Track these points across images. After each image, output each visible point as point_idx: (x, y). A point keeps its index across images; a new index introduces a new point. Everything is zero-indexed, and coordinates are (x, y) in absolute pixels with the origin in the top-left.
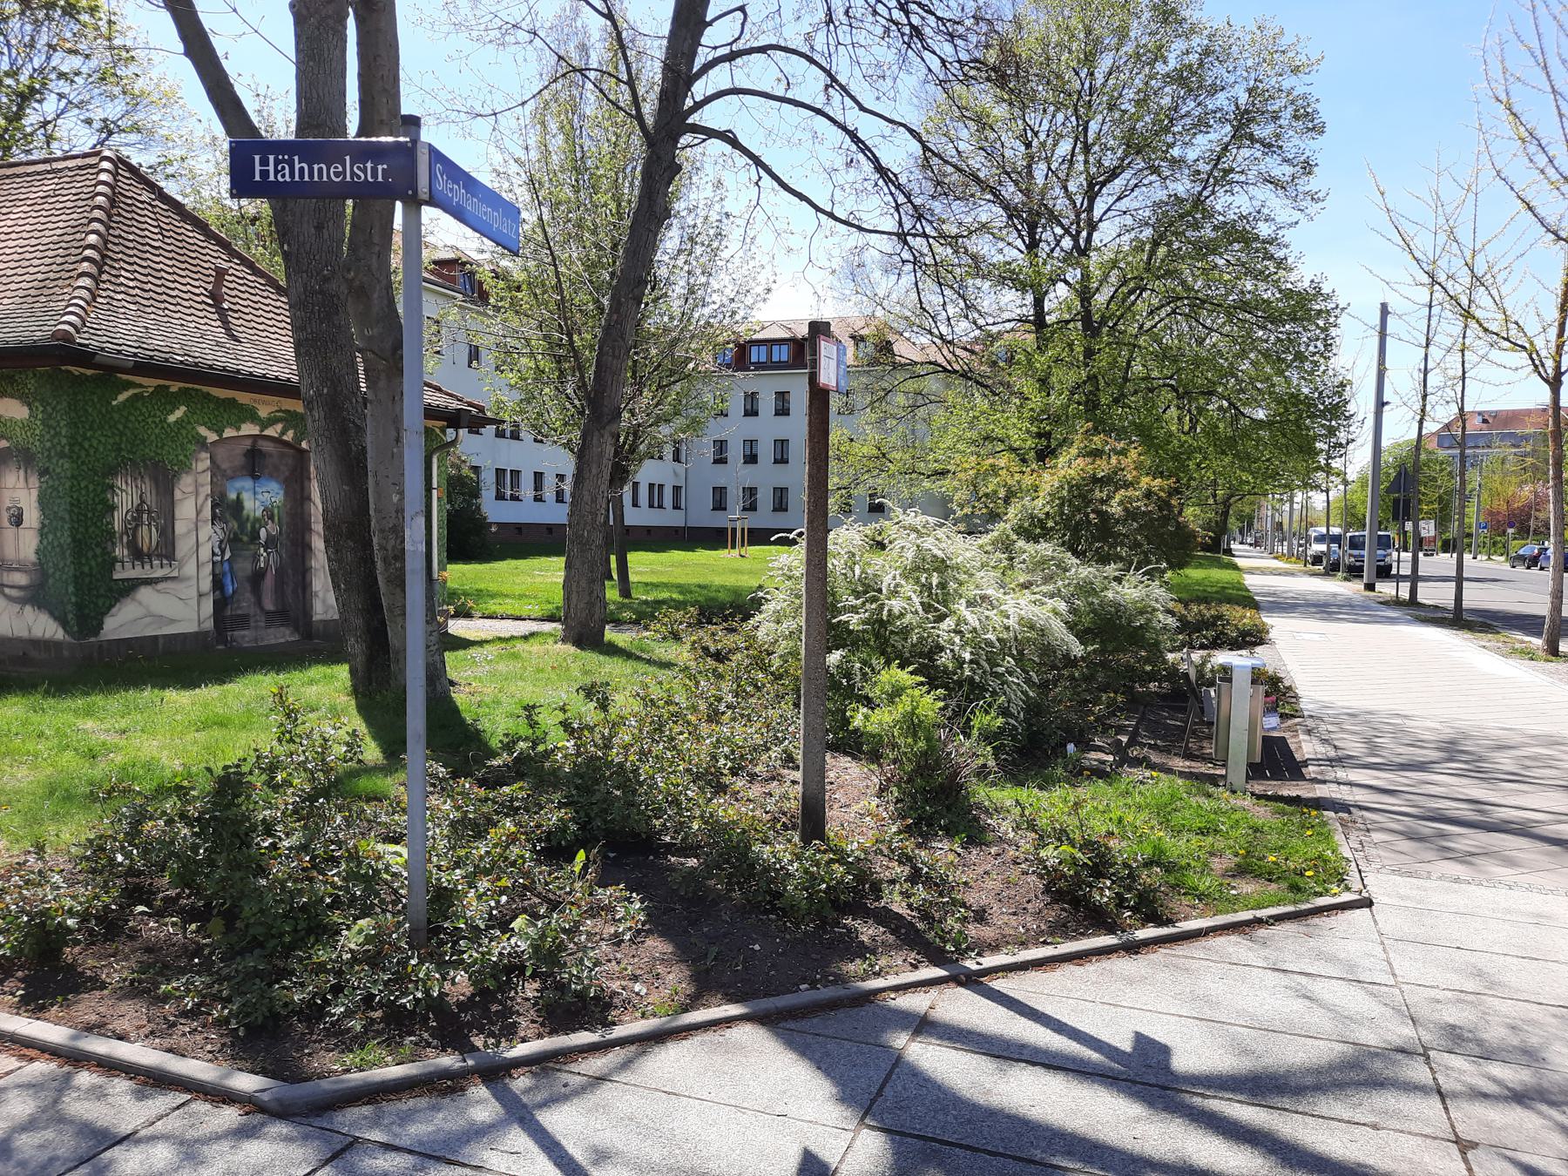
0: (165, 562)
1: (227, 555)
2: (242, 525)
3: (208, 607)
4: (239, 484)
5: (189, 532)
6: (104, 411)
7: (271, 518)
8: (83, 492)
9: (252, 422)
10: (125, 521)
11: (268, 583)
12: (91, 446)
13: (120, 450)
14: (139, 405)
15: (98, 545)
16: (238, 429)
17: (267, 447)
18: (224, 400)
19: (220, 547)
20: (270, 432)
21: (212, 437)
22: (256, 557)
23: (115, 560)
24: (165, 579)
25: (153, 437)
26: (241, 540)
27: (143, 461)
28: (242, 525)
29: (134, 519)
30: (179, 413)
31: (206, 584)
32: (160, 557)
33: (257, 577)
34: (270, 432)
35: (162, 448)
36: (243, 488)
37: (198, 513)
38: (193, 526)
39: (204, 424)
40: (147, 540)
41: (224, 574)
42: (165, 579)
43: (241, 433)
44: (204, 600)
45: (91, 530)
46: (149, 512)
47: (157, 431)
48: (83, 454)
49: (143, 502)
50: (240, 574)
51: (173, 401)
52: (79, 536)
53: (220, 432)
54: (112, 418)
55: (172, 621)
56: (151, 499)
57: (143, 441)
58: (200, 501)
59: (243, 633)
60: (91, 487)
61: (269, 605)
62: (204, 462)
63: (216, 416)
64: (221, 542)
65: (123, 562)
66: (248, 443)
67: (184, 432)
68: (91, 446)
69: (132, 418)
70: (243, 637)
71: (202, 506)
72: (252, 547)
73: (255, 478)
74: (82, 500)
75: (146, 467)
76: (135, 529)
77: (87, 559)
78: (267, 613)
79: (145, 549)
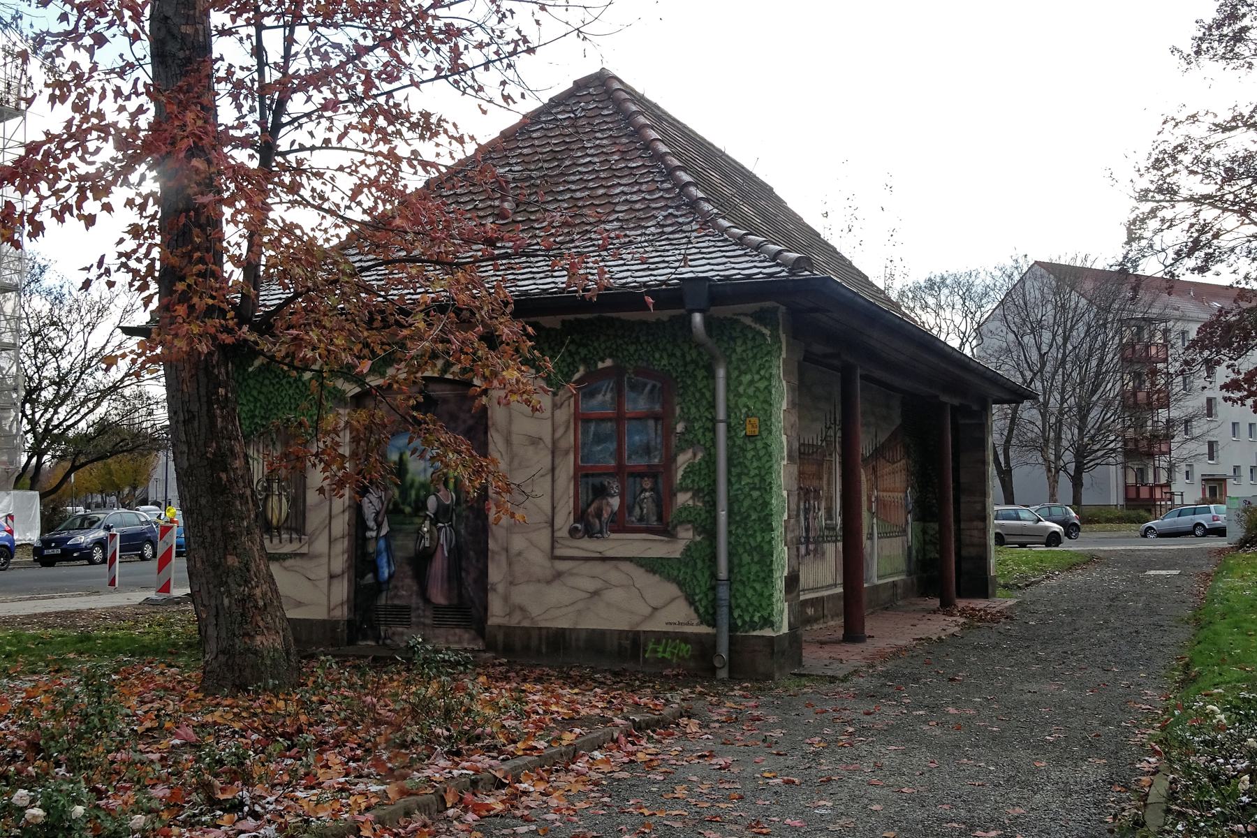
0: (294, 536)
2: (404, 491)
3: (341, 590)
4: (402, 441)
11: (438, 566)
19: (376, 520)
24: (294, 555)
25: (286, 400)
26: (402, 512)
28: (404, 491)
32: (290, 529)
33: (421, 561)
40: (276, 511)
41: (379, 553)
42: (294, 555)
44: (335, 582)
47: (291, 392)
50: (399, 554)
54: (248, 385)
64: (377, 513)
78: (437, 608)
79: (275, 521)
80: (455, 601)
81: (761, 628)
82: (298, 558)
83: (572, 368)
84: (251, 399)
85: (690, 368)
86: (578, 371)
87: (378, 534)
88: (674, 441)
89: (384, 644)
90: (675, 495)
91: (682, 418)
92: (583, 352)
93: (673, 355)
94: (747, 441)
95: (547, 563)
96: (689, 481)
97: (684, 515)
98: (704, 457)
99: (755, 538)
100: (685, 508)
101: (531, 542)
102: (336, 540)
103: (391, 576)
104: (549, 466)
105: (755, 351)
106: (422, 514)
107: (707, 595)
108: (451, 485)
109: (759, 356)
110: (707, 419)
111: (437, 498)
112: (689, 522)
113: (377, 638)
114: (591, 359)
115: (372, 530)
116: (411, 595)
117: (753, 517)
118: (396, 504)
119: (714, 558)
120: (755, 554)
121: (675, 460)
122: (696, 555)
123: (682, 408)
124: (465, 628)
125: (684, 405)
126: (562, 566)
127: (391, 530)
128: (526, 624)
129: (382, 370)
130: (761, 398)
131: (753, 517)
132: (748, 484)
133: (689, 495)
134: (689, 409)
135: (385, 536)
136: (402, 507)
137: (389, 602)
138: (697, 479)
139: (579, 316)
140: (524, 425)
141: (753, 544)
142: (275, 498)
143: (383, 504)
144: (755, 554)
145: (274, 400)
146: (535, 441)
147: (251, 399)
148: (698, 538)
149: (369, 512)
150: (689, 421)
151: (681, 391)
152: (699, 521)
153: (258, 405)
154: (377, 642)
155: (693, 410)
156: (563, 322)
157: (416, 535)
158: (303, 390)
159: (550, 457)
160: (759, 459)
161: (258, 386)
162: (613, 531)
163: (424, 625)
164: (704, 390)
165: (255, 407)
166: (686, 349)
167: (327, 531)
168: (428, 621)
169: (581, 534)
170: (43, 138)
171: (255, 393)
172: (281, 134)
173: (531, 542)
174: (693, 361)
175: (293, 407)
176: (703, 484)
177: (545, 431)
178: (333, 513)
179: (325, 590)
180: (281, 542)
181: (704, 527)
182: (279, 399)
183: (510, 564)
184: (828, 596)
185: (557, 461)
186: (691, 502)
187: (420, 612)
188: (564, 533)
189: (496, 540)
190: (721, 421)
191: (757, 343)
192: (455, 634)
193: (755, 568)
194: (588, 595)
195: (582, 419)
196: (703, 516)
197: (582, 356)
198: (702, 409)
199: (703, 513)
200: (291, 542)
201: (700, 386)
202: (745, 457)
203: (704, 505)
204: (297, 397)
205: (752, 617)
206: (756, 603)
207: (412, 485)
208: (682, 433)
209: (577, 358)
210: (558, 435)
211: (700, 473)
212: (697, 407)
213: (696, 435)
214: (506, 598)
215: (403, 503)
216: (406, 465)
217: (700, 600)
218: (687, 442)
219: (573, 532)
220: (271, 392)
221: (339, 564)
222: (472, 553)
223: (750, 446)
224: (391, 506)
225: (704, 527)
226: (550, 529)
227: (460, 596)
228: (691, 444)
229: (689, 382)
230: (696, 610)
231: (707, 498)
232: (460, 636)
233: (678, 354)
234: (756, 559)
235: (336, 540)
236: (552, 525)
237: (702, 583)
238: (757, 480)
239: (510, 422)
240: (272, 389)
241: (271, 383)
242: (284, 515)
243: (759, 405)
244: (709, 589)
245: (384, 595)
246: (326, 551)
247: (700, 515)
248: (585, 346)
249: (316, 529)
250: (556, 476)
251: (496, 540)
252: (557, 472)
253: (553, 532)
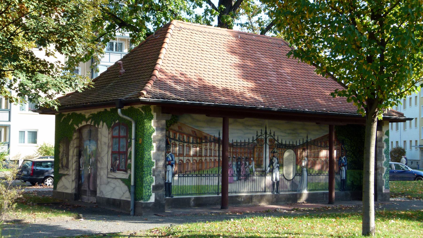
126: (109, 180)
146: (105, 143)
156: (111, 109)
160: (142, 150)
162: (118, 170)
170: (43, 60)
172: (125, 55)
184: (255, 195)
221: (73, 177)
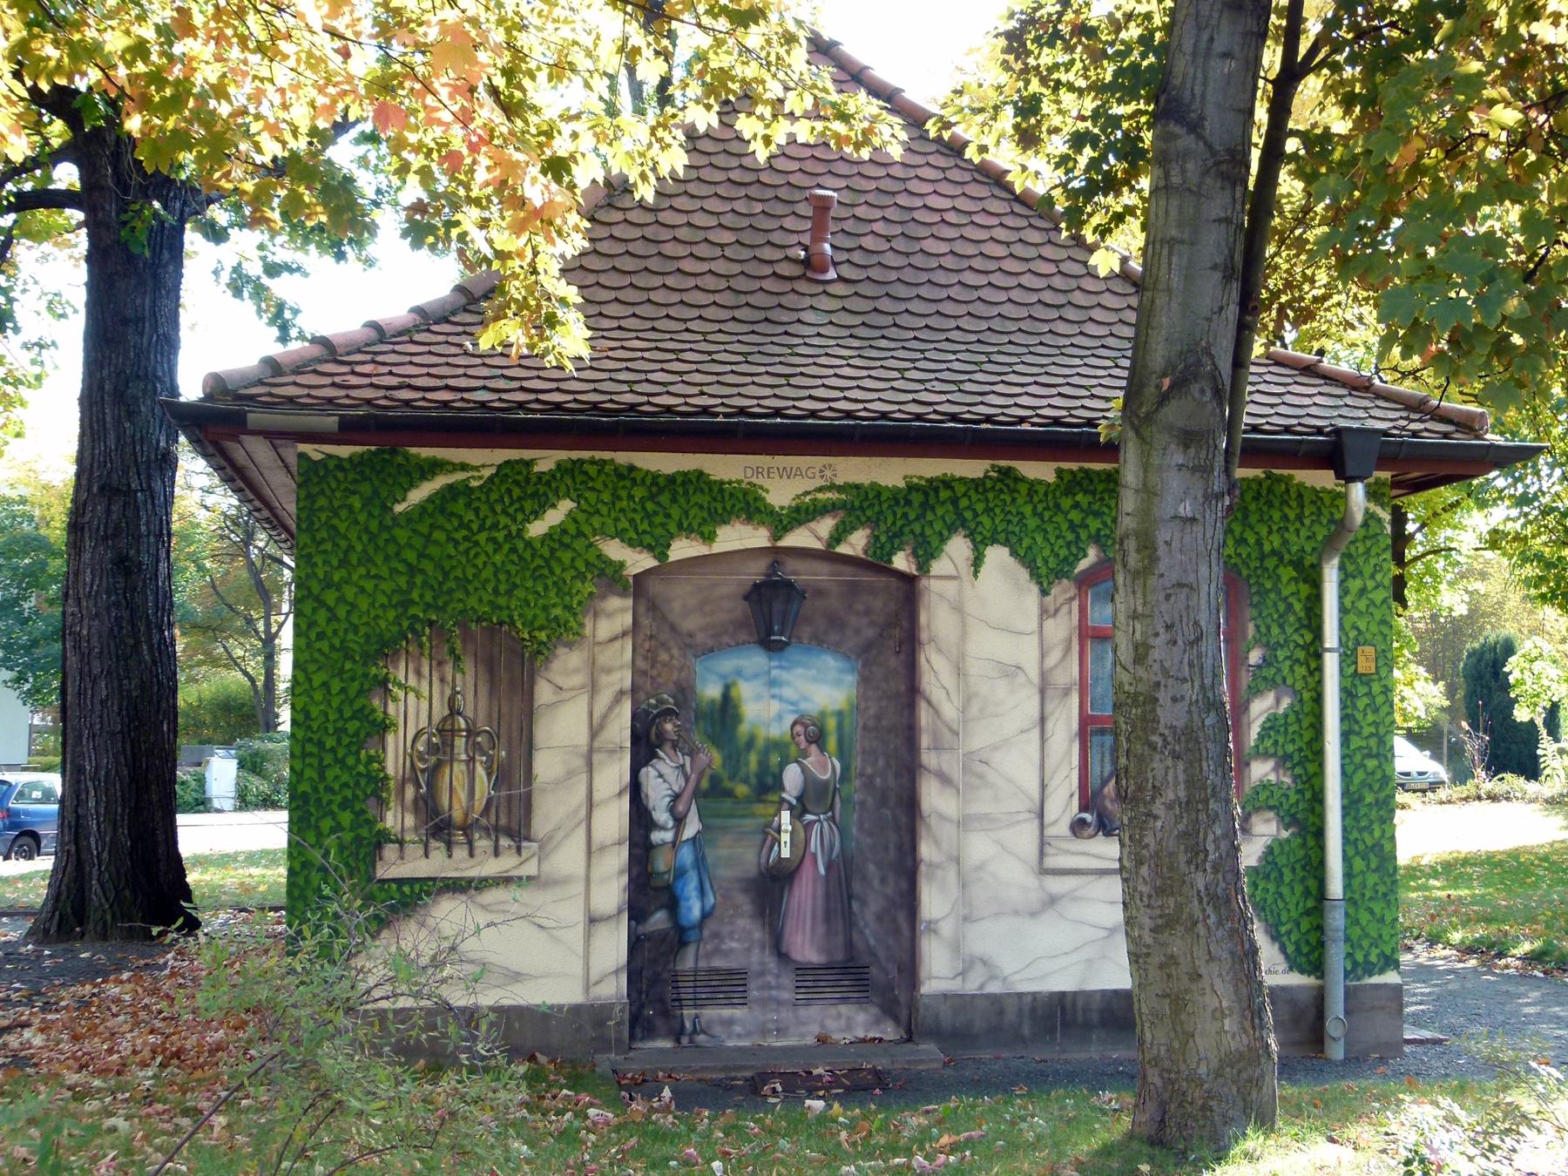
1: (692, 828)
3: (613, 947)
4: (727, 664)
5: (570, 774)
6: (374, 526)
7: (818, 739)
8: (318, 696)
9: (749, 519)
10: (412, 756)
11: (805, 897)
12: (341, 599)
13: (406, 603)
14: (459, 506)
15: (345, 805)
16: (709, 538)
17: (803, 574)
18: (671, 479)
20: (799, 538)
21: (638, 561)
22: (769, 834)
23: (382, 838)
24: (505, 880)
26: (729, 794)
27: (464, 626)
28: (734, 759)
29: (432, 749)
30: (555, 516)
31: (611, 892)
32: (495, 831)
34: (799, 538)
35: (509, 592)
36: (739, 673)
37: (594, 732)
38: (579, 763)
39: (620, 535)
40: (462, 794)
41: (680, 873)
42: (505, 880)
43: (718, 547)
45: (330, 774)
46: (471, 732)
47: (498, 558)
48: (322, 616)
49: (454, 711)
50: (724, 873)
51: (540, 493)
52: (304, 787)
53: (659, 548)
54: (393, 540)
55: (517, 977)
56: (475, 704)
57: (463, 583)
58: (599, 709)
59: (727, 1012)
60: (336, 686)
61: (806, 947)
62: (617, 614)
63: (648, 516)
64: (676, 797)
65: (401, 843)
66: (755, 571)
67: (566, 556)
68: (341, 599)
69: (439, 536)
70: (730, 1022)
71: (605, 717)
72: (759, 808)
73: (770, 645)
74: (314, 712)
75: (467, 636)
76: (434, 772)
77: (319, 834)
78: (802, 969)
79: (457, 815)
80: (839, 956)
81: (1381, 972)
82: (513, 887)
83: (1074, 550)
84: (401, 567)
85: (1271, 563)
86: (1085, 556)
87: (677, 835)
88: (1245, 679)
89: (693, 1045)
90: (1248, 764)
91: (1257, 642)
92: (1094, 524)
93: (1241, 541)
94: (1357, 682)
95: (1031, 881)
96: (1268, 743)
97: (1263, 796)
98: (1292, 706)
99: (1371, 832)
100: (1264, 786)
101: (1004, 848)
102: (603, 848)
103: (706, 915)
104: (1036, 714)
105: (1368, 543)
106: (775, 798)
107: (1298, 925)
108: (832, 743)
109: (1373, 552)
110: (1297, 645)
111: (804, 770)
112: (1271, 808)
113: (677, 1034)
114: (1108, 537)
115: (663, 828)
116: (749, 950)
117: (1368, 800)
118: (715, 780)
119: (1317, 868)
120: (1372, 856)
121: (1247, 709)
122: (1282, 860)
123: (1257, 627)
124: (858, 1001)
125: (1259, 622)
126: (1057, 885)
127: (706, 828)
128: (994, 988)
129: (706, 529)
130: (1378, 617)
131: (1368, 800)
132: (1360, 748)
133: (1270, 764)
134: (1268, 628)
135: (694, 839)
136: (728, 784)
137: (702, 964)
138: (1281, 740)
139: (1087, 465)
140: (986, 646)
141: (1369, 842)
142: (459, 769)
143: (687, 780)
144: (1372, 856)
145: (459, 573)
146: (1010, 671)
147: (401, 567)
148: (1285, 834)
149: (658, 789)
150: (1272, 648)
151: (1256, 599)
152: (1286, 807)
153: (419, 580)
154: (678, 1041)
155: (1275, 630)
156: (1060, 473)
157: (759, 837)
158: (527, 555)
159: (1036, 700)
160: (1376, 711)
161: (418, 542)
163: (779, 1002)
164: (1291, 600)
165: (411, 585)
166: (1264, 531)
167: (582, 831)
168: (785, 995)
169: (1091, 830)
171: (411, 556)
173: (1004, 848)
174: (1274, 552)
175: (503, 588)
176: (1290, 748)
177: (1027, 654)
178: (597, 797)
179: (579, 948)
180: (471, 855)
181: (1293, 816)
182: (470, 572)
183: (963, 885)
185: (1049, 707)
186: (1272, 777)
187: (770, 978)
188: (1063, 828)
189: (937, 843)
190: (1330, 650)
191: (1371, 532)
192: (839, 1015)
193: (1372, 879)
194: (1104, 933)
195: (1089, 635)
196: (1293, 798)
197: (1093, 530)
198: (1289, 630)
199: (1291, 793)
200: (497, 853)
201: (1286, 592)
202: (1355, 707)
203: (1294, 781)
204: (513, 569)
205: (1366, 956)
206: (1374, 934)
207: (750, 744)
208: (1259, 667)
209: (1083, 535)
210: (1052, 660)
211: (1286, 732)
212: (1281, 626)
213: (1279, 670)
214: (956, 947)
215: (732, 777)
216: (736, 707)
217: (1289, 933)
218: (1266, 680)
219: (1078, 827)
220: (450, 557)
222: (871, 867)
223: (1362, 690)
224: (705, 784)
225: (1293, 816)
226: (1036, 823)
227: (849, 945)
228: (1272, 684)
229: (1268, 585)
230: (1283, 949)
231: (1298, 770)
232: (849, 1019)
233: (1251, 540)
234: (1373, 865)
235: (603, 848)
236: (1041, 816)
237: (1292, 907)
238: (1373, 742)
239: (964, 636)
240: (452, 552)
241: (450, 539)
242: (479, 805)
243: (1374, 628)
244: (1301, 915)
245: (690, 951)
246: (581, 871)
247: (1287, 796)
248: (1097, 514)
249: (558, 829)
250: (1049, 732)
251: (937, 843)
252: (1049, 725)
253: (1042, 827)
